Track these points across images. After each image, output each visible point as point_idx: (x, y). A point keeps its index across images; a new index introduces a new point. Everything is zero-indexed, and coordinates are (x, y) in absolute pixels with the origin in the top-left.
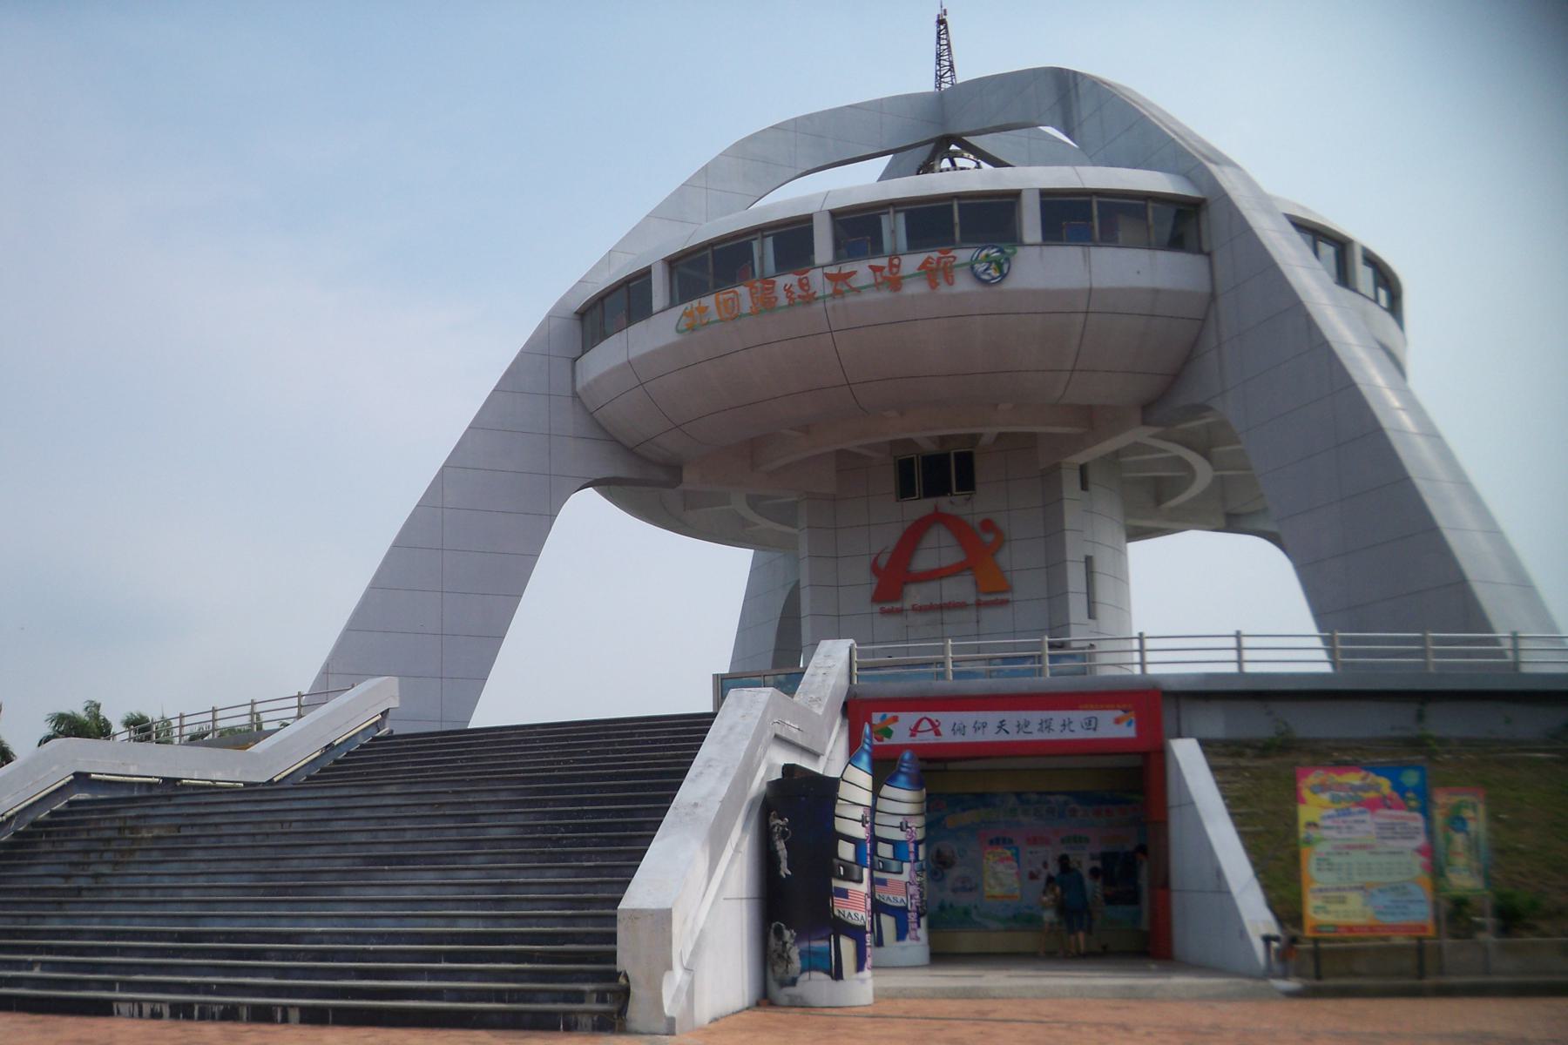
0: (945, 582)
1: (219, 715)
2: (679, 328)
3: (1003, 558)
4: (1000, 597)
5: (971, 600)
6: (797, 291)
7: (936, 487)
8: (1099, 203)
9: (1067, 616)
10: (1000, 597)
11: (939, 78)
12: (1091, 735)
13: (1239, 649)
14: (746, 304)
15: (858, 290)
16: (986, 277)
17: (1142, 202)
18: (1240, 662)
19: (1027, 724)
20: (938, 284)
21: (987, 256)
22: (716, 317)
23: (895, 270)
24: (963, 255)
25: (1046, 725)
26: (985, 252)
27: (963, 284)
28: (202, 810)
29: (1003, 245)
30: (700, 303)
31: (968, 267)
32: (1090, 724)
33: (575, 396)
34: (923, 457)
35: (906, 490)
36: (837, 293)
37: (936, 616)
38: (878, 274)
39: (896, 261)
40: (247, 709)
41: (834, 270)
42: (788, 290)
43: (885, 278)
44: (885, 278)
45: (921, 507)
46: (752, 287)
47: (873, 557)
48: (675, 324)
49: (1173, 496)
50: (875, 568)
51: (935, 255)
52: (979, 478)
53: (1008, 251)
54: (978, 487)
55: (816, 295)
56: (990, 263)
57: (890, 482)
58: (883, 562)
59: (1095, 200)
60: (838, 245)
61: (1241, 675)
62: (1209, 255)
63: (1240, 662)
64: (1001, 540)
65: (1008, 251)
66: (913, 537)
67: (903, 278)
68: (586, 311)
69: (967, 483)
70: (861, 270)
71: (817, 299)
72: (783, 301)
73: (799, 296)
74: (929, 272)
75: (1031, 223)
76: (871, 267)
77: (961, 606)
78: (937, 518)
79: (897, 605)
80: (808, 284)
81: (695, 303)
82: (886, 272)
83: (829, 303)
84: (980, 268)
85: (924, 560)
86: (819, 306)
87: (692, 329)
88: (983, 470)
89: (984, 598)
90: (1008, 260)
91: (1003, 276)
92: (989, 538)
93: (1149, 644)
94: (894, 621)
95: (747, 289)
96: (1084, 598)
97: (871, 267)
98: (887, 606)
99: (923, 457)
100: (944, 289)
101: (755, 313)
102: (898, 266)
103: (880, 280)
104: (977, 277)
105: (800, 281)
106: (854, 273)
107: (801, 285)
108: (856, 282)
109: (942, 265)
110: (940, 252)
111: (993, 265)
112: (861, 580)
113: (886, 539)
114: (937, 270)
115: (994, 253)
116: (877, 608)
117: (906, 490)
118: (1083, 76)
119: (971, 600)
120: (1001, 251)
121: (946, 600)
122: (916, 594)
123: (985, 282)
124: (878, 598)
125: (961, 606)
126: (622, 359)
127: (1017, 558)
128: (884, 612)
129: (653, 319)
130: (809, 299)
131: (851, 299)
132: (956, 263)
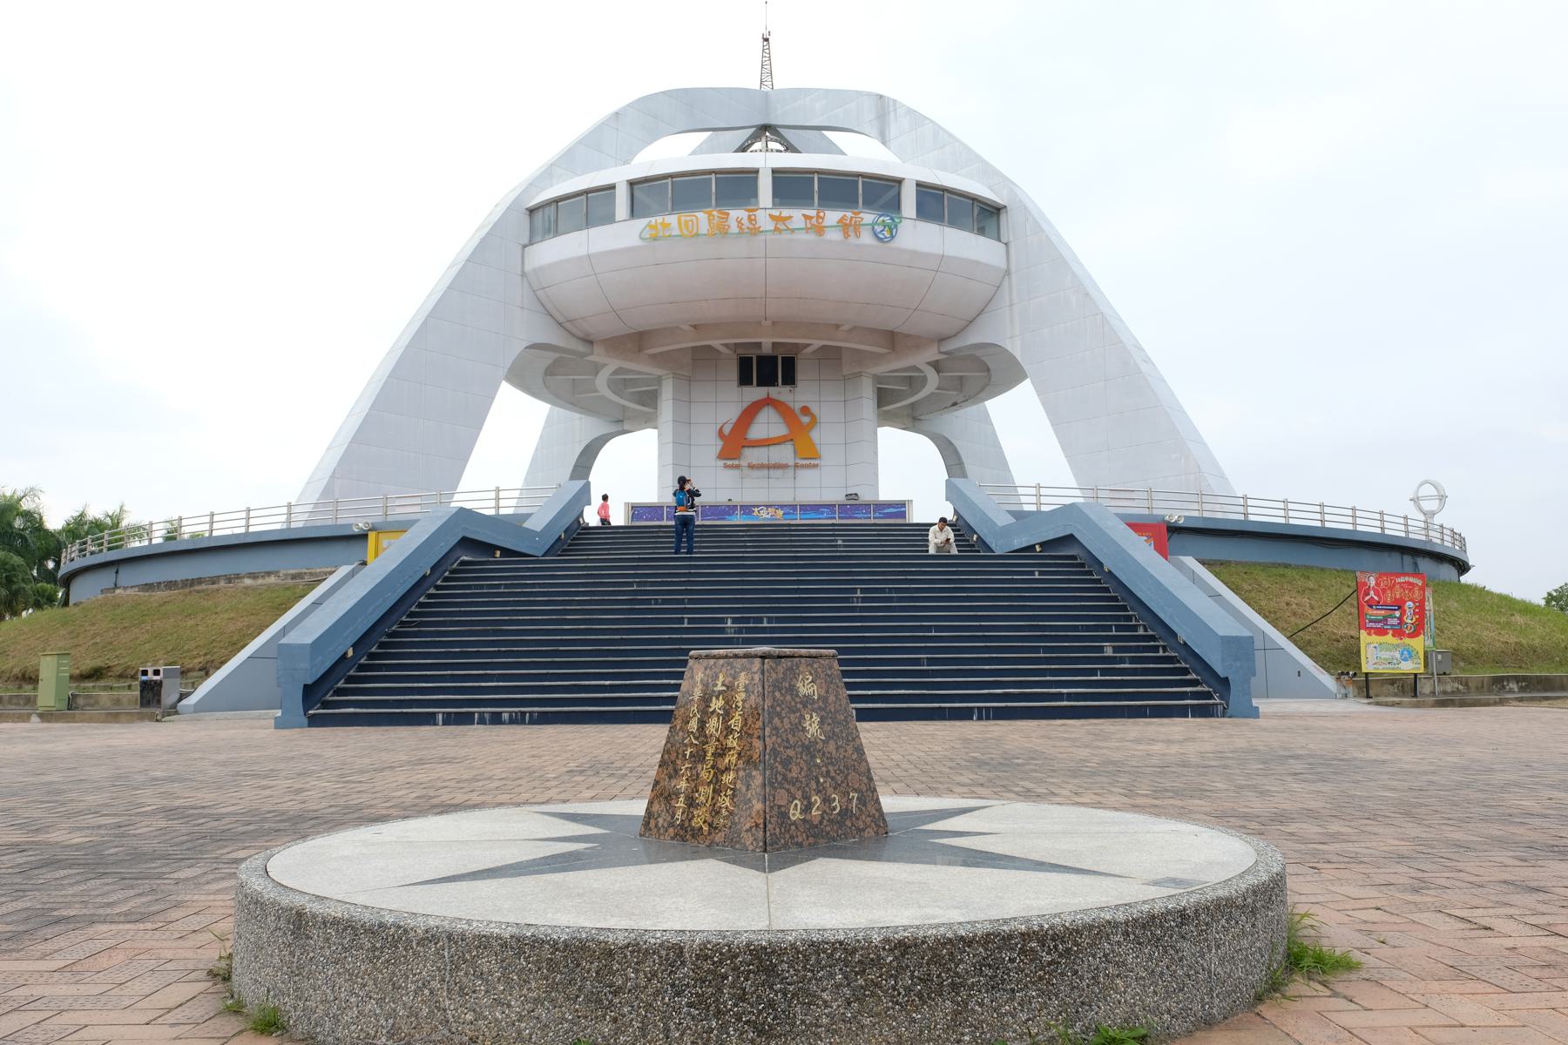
0: (772, 448)
1: (252, 514)
2: (643, 236)
4: (813, 462)
5: (791, 463)
6: (745, 221)
7: (767, 380)
8: (863, 182)
13: (498, 499)
14: (704, 228)
15: (793, 231)
16: (881, 236)
17: (942, 193)
18: (497, 507)
20: (849, 236)
21: (883, 221)
22: (676, 232)
23: (820, 220)
26: (882, 218)
27: (866, 238)
29: (893, 215)
30: (664, 219)
31: (871, 227)
33: (523, 274)
34: (794, 358)
35: (745, 380)
37: (765, 472)
38: (808, 221)
39: (822, 214)
41: (776, 213)
42: (739, 222)
43: (812, 225)
45: (756, 393)
46: (709, 214)
47: (719, 426)
48: (639, 233)
49: (889, 404)
50: (721, 434)
51: (849, 214)
52: (799, 376)
53: (897, 220)
54: (799, 383)
55: (761, 229)
56: (885, 227)
57: (734, 374)
58: (727, 430)
59: (860, 180)
60: (775, 195)
61: (1383, 535)
63: (1407, 532)
64: (814, 421)
65: (897, 220)
68: (538, 209)
69: (790, 380)
70: (797, 215)
71: (762, 232)
72: (734, 229)
73: (748, 228)
74: (844, 226)
75: (765, 185)
76: (804, 215)
77: (783, 467)
78: (768, 402)
79: (736, 462)
80: (755, 220)
81: (659, 219)
82: (814, 220)
83: (769, 236)
84: (878, 229)
85: (758, 430)
86: (761, 237)
90: (896, 226)
91: (892, 237)
92: (805, 420)
93: (502, 495)
95: (706, 215)
97: (804, 215)
98: (730, 462)
99: (794, 358)
100: (852, 239)
101: (711, 235)
102: (823, 218)
103: (809, 226)
105: (749, 216)
109: (853, 222)
110: (853, 213)
111: (887, 228)
113: (729, 413)
114: (850, 225)
115: (887, 219)
116: (721, 463)
117: (745, 380)
119: (791, 463)
120: (892, 219)
122: (752, 455)
123: (880, 240)
124: (722, 456)
125: (783, 467)
126: (583, 252)
128: (726, 466)
129: (615, 225)
130: (755, 231)
131: (786, 236)
132: (864, 222)
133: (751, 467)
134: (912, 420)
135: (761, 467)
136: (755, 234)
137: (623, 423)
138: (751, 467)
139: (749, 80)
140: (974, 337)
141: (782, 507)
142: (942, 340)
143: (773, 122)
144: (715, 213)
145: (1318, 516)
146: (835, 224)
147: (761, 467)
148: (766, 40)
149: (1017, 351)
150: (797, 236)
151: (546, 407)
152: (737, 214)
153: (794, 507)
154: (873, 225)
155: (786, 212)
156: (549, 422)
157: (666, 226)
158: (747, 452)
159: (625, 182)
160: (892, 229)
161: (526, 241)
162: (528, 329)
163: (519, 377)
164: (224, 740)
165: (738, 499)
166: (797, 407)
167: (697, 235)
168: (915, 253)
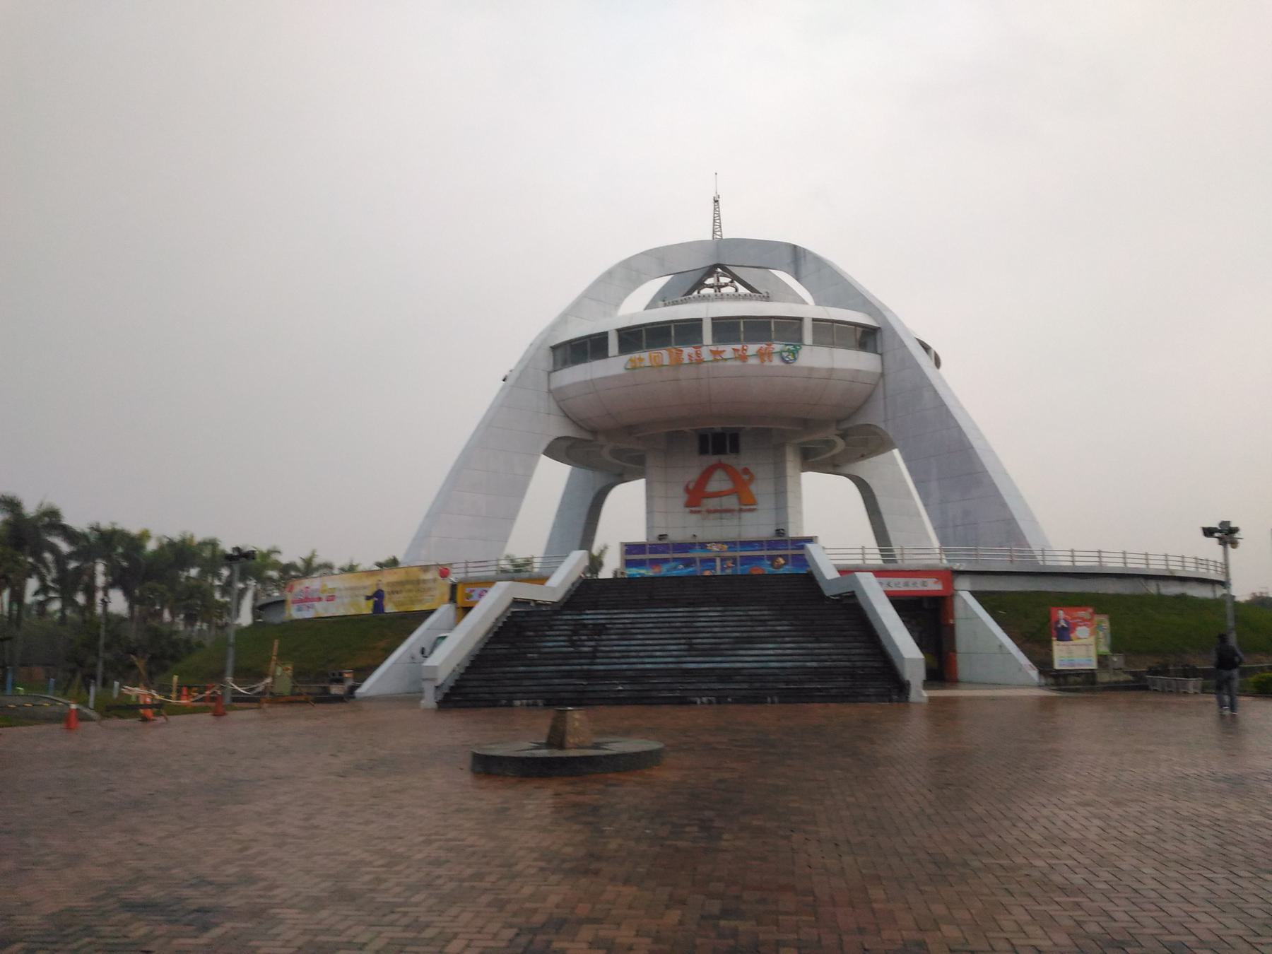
3: (754, 488)
4: (752, 507)
6: (694, 355)
7: (719, 450)
9: (787, 518)
10: (752, 507)
11: (714, 232)
12: (925, 589)
14: (666, 361)
15: (726, 360)
19: (899, 583)
20: (765, 361)
22: (648, 364)
23: (744, 352)
24: (777, 347)
25: (906, 584)
27: (776, 361)
28: (739, 629)
32: (906, 584)
35: (703, 451)
36: (715, 360)
37: (718, 515)
40: (463, 565)
41: (714, 348)
44: (740, 355)
45: (713, 459)
50: (687, 490)
51: (764, 346)
58: (691, 487)
62: (881, 354)
64: (752, 478)
66: (706, 476)
67: (748, 356)
70: (728, 350)
72: (686, 361)
76: (733, 349)
78: (720, 466)
84: (785, 354)
87: (634, 368)
88: (744, 441)
89: (744, 507)
91: (795, 359)
92: (746, 477)
94: (694, 517)
96: (1161, 584)
98: (693, 509)
100: (767, 363)
103: (737, 356)
104: (783, 359)
105: (696, 352)
106: (724, 351)
107: (697, 354)
108: (725, 356)
112: (682, 497)
113: (693, 475)
115: (791, 348)
116: (688, 509)
118: (810, 253)
119: (736, 507)
121: (724, 508)
122: (712, 503)
123: (787, 362)
124: (688, 505)
127: (761, 488)
128: (692, 512)
130: (700, 361)
131: (721, 363)
132: (774, 351)
133: (709, 512)
134: (832, 466)
135: (716, 511)
136: (700, 363)
137: (622, 478)
138: (709, 512)
139: (703, 233)
140: (861, 420)
141: (726, 543)
142: (839, 421)
143: (721, 263)
144: (674, 350)
145: (1070, 559)
146: (755, 353)
147: (716, 511)
148: (716, 201)
149: (891, 433)
150: (729, 363)
151: (570, 467)
152: (688, 351)
153: (734, 543)
154: (780, 353)
155: (721, 348)
156: (572, 475)
157: (641, 360)
158: (705, 501)
159: (614, 331)
160: (794, 353)
161: (551, 368)
162: (558, 428)
163: (552, 452)
164: (1085, 625)
165: (700, 538)
166: (739, 468)
167: (663, 366)
168: (811, 369)
